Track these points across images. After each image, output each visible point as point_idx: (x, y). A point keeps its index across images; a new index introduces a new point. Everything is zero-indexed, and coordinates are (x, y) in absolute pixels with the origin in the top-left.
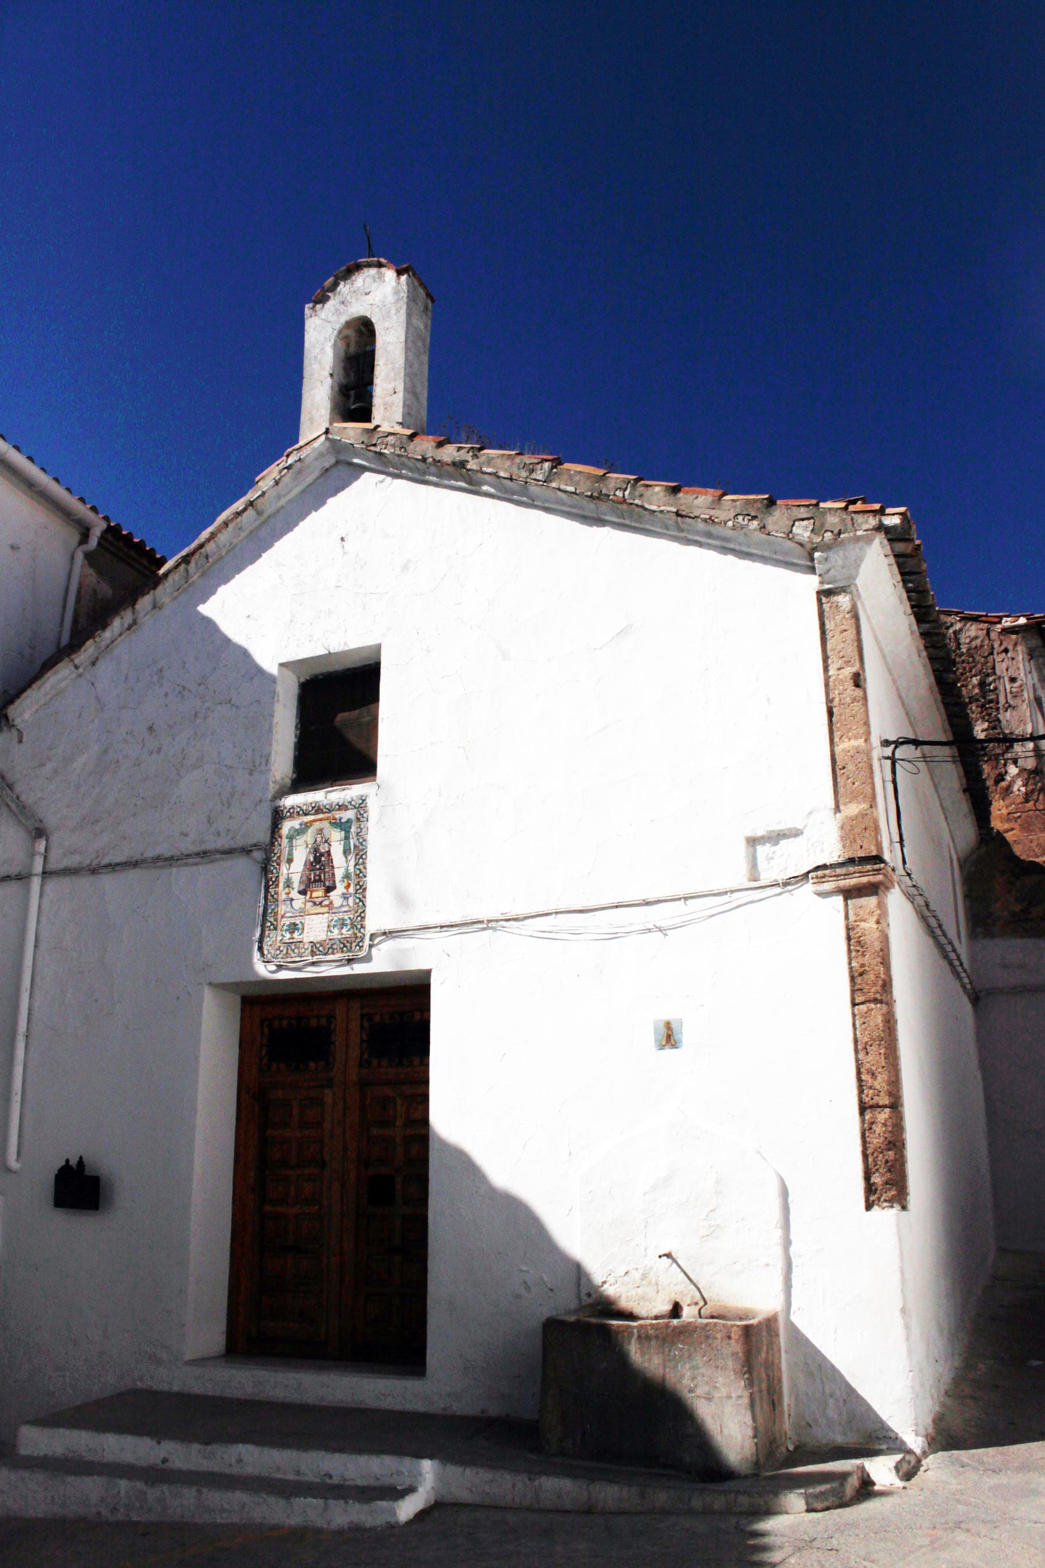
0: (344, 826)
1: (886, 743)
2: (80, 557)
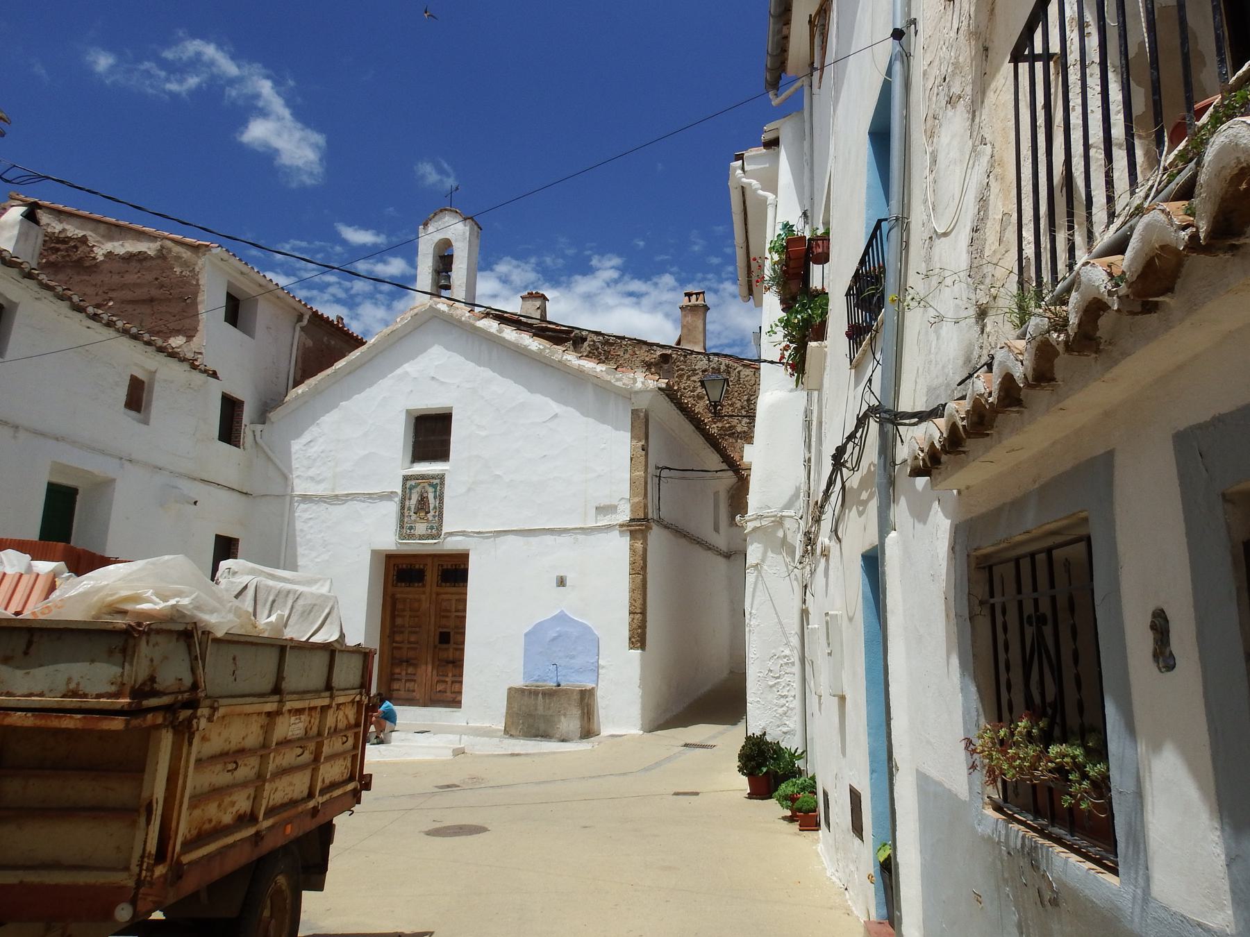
0: (435, 486)
1: (657, 468)
2: (298, 329)
